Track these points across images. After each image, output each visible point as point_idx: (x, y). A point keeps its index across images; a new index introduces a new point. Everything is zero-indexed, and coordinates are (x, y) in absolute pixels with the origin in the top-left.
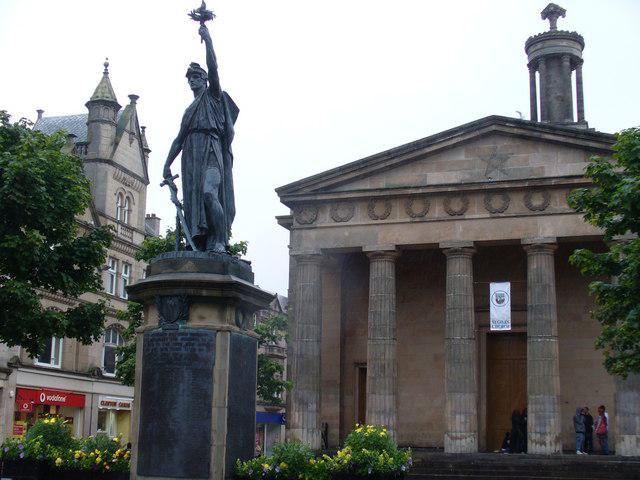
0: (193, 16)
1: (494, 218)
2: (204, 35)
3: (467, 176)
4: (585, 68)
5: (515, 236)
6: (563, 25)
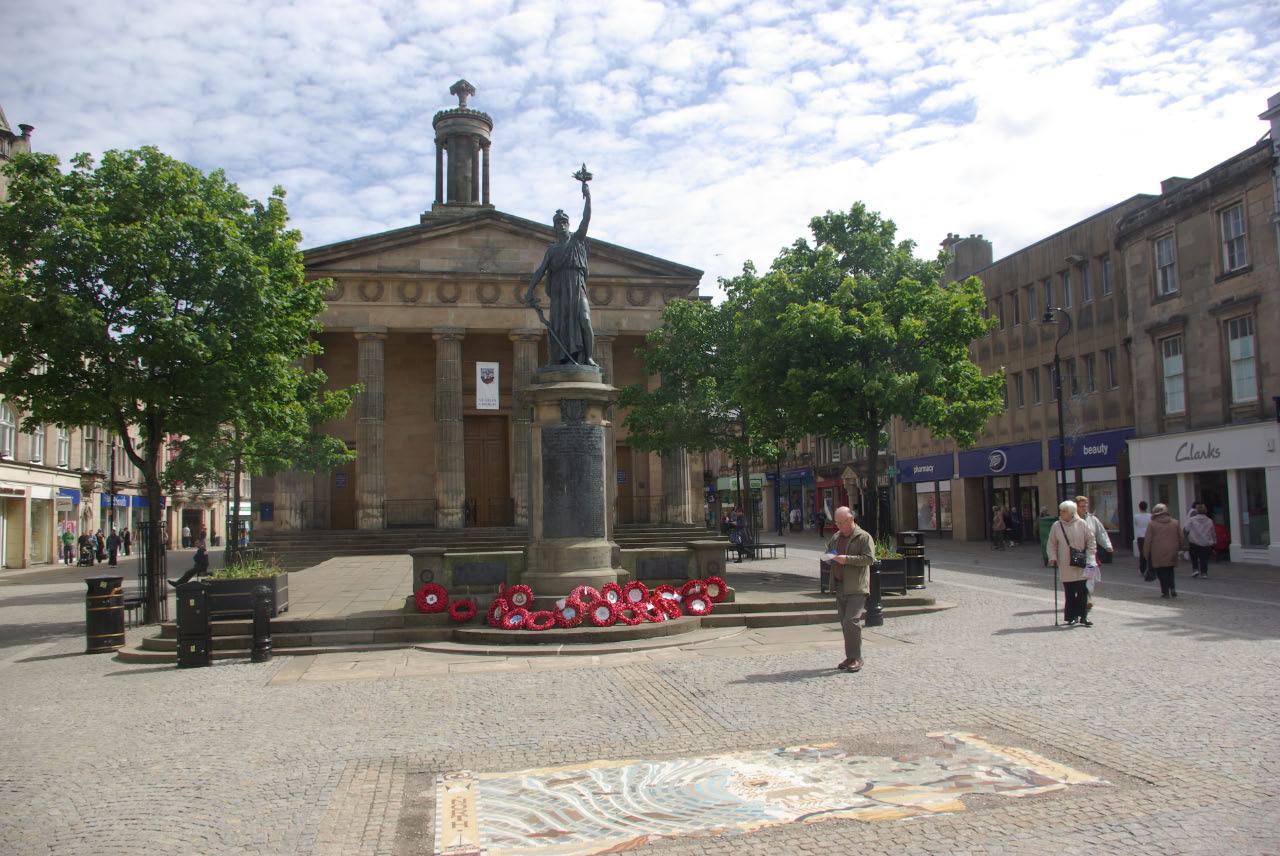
0: (577, 176)
1: (485, 307)
2: (586, 193)
3: (460, 265)
4: (492, 149)
5: (506, 325)
6: (471, 104)
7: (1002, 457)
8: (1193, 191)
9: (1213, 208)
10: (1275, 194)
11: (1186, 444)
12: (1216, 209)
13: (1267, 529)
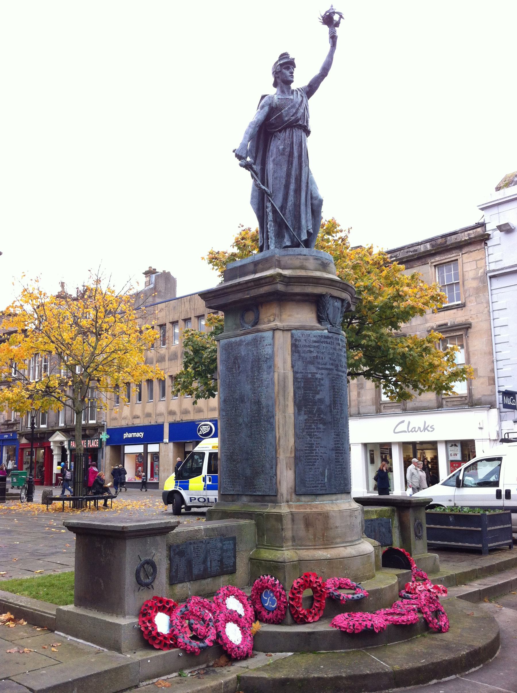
2: (333, 38)
7: (211, 428)
8: (415, 251)
9: (432, 263)
10: (487, 258)
11: (403, 422)
12: (434, 264)
13: (432, 485)
